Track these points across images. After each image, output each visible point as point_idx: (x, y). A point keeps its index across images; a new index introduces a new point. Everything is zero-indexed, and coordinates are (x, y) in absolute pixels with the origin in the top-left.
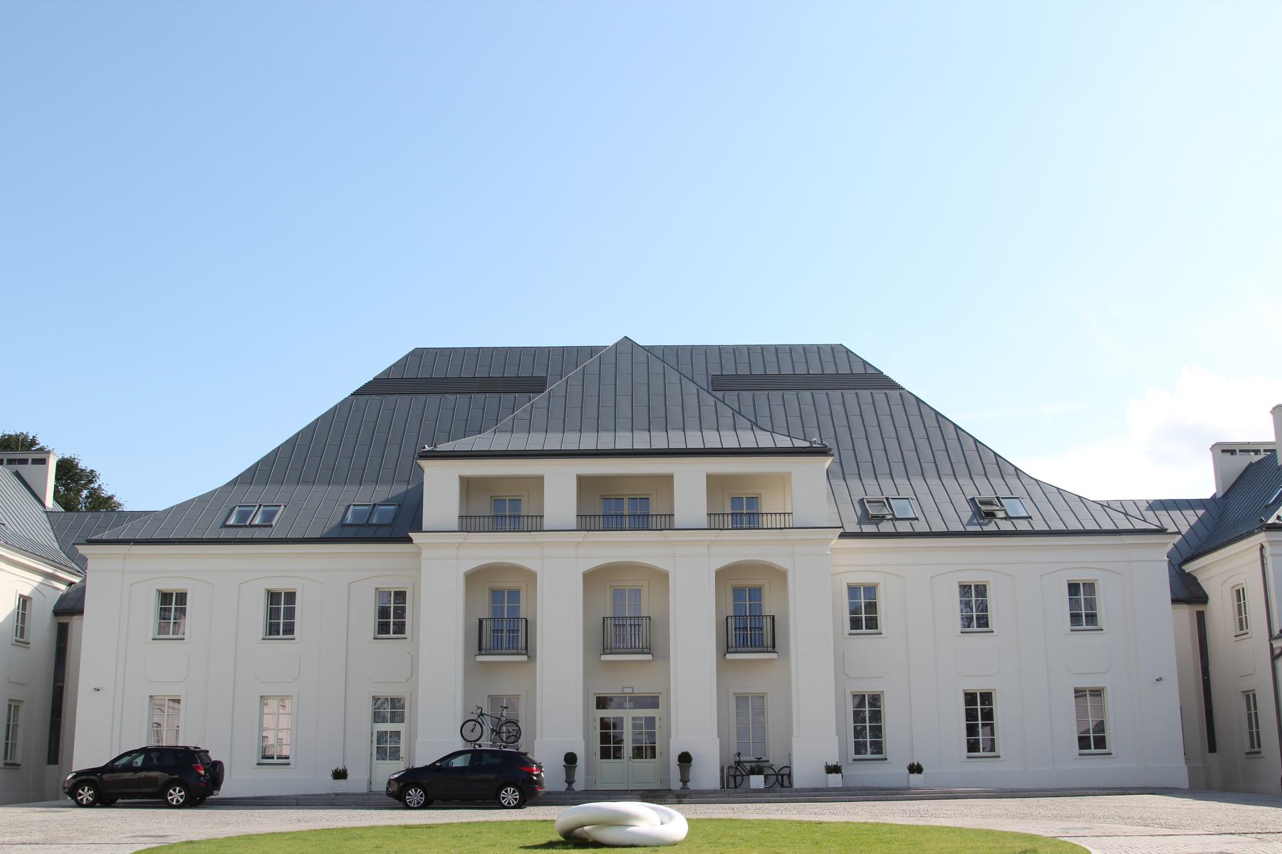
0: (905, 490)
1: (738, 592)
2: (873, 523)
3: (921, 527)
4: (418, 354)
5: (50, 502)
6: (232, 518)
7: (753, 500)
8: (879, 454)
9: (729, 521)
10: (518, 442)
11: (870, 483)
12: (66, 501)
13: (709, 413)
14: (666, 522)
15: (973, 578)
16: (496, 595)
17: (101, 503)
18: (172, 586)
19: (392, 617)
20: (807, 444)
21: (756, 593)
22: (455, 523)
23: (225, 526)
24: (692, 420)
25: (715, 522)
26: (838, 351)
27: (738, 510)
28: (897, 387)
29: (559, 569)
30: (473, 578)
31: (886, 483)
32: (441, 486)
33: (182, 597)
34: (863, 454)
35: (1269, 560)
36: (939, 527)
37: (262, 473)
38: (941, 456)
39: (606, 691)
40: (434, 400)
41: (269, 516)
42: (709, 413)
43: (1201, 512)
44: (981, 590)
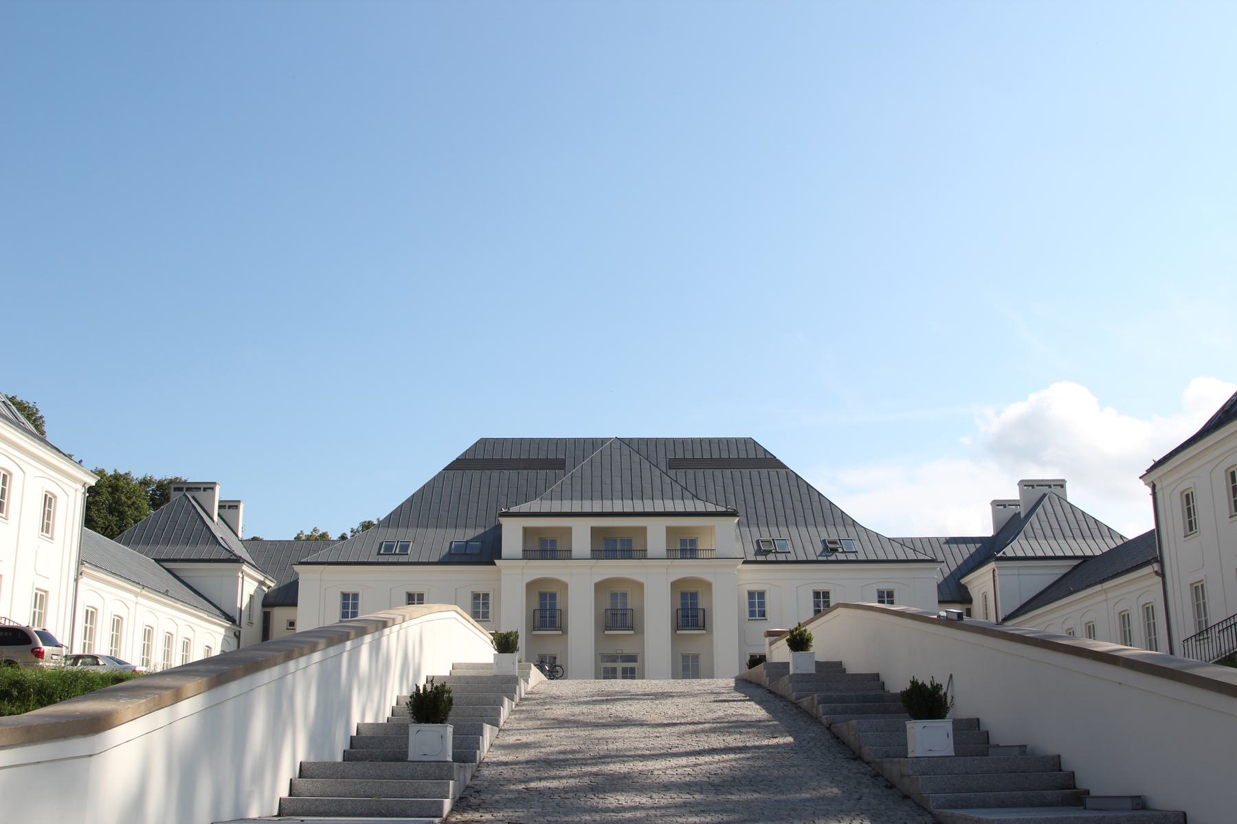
0: (785, 535)
1: (684, 595)
2: (764, 554)
3: (791, 557)
4: (483, 442)
7: (693, 542)
8: (771, 511)
10: (556, 507)
11: (764, 529)
13: (667, 488)
14: (643, 555)
15: (821, 588)
20: (724, 509)
21: (694, 596)
23: (379, 554)
24: (657, 493)
25: (671, 555)
26: (749, 443)
27: (685, 548)
28: (785, 467)
31: (774, 529)
32: (512, 534)
34: (761, 511)
35: (997, 578)
36: (802, 557)
37: (397, 518)
38: (808, 512)
39: (611, 649)
42: (667, 488)
43: (978, 545)
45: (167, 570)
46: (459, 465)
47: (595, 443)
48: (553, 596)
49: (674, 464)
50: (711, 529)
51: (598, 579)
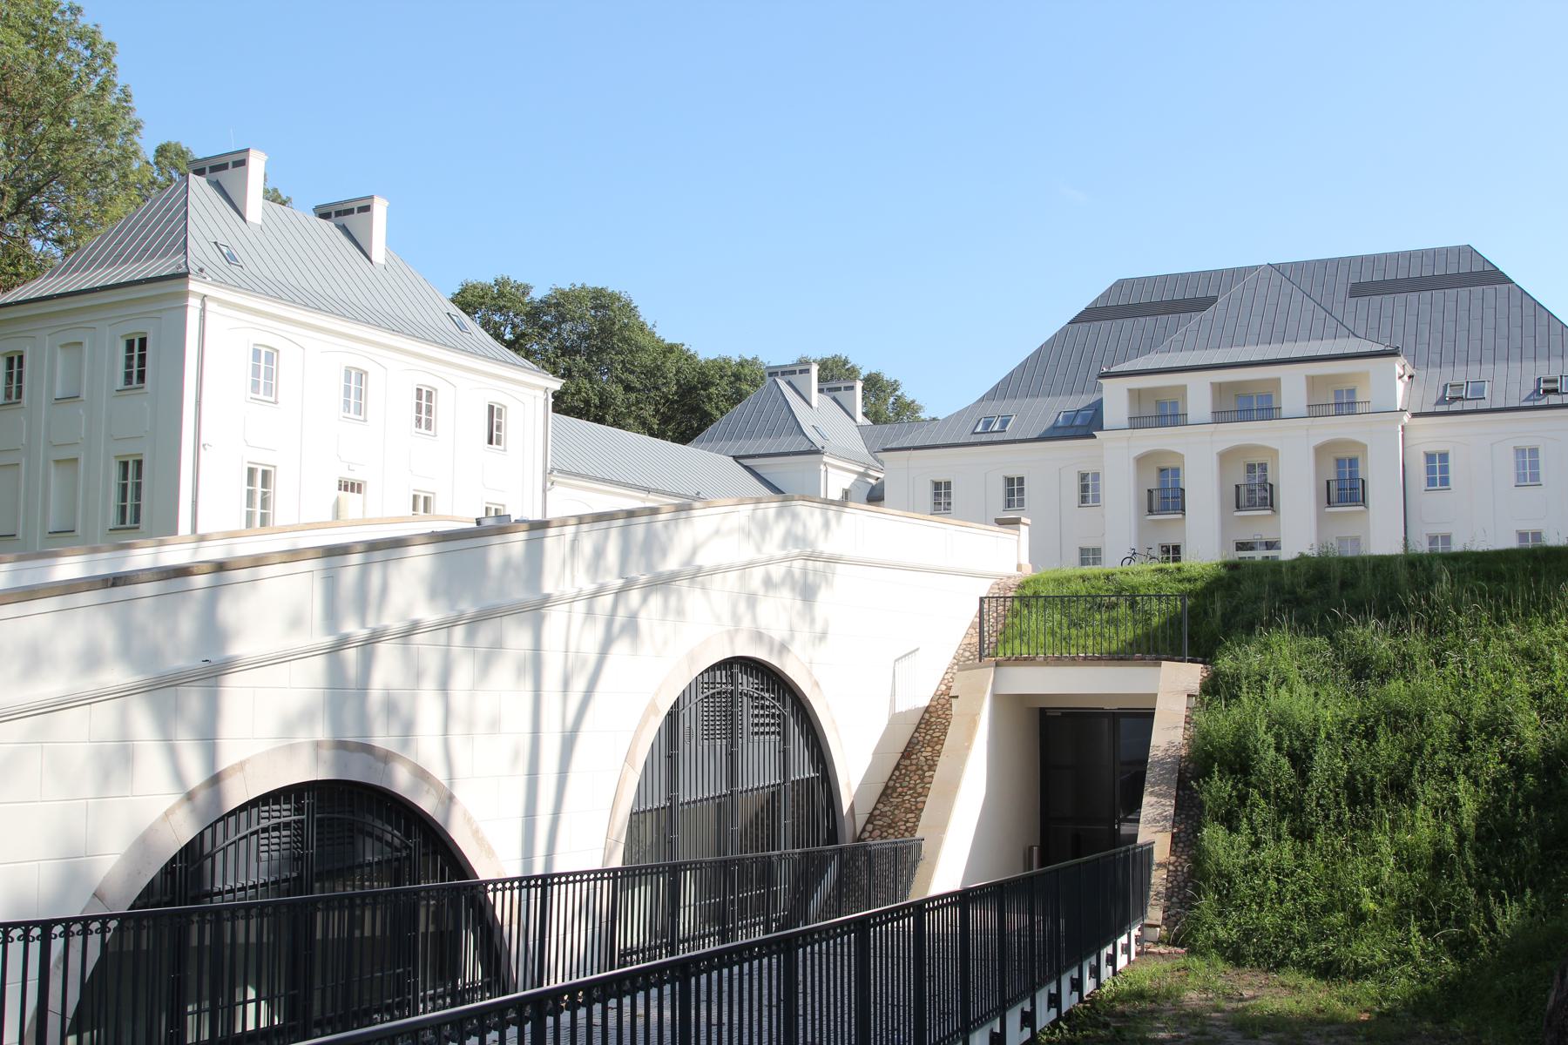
2: (1451, 404)
4: (1120, 284)
5: (860, 418)
6: (983, 428)
7: (1352, 392)
9: (1332, 410)
12: (874, 416)
15: (1526, 443)
16: (1339, 462)
17: (905, 409)
19: (1088, 490)
22: (1126, 424)
26: (1471, 251)
29: (1200, 451)
30: (1321, 451)
32: (1116, 398)
33: (948, 485)
37: (1001, 391)
39: (1245, 537)
40: (1128, 322)
41: (1005, 424)
44: (1534, 452)
45: (746, 467)
46: (1090, 315)
47: (1236, 275)
48: (1263, 467)
49: (1359, 290)
51: (1319, 441)
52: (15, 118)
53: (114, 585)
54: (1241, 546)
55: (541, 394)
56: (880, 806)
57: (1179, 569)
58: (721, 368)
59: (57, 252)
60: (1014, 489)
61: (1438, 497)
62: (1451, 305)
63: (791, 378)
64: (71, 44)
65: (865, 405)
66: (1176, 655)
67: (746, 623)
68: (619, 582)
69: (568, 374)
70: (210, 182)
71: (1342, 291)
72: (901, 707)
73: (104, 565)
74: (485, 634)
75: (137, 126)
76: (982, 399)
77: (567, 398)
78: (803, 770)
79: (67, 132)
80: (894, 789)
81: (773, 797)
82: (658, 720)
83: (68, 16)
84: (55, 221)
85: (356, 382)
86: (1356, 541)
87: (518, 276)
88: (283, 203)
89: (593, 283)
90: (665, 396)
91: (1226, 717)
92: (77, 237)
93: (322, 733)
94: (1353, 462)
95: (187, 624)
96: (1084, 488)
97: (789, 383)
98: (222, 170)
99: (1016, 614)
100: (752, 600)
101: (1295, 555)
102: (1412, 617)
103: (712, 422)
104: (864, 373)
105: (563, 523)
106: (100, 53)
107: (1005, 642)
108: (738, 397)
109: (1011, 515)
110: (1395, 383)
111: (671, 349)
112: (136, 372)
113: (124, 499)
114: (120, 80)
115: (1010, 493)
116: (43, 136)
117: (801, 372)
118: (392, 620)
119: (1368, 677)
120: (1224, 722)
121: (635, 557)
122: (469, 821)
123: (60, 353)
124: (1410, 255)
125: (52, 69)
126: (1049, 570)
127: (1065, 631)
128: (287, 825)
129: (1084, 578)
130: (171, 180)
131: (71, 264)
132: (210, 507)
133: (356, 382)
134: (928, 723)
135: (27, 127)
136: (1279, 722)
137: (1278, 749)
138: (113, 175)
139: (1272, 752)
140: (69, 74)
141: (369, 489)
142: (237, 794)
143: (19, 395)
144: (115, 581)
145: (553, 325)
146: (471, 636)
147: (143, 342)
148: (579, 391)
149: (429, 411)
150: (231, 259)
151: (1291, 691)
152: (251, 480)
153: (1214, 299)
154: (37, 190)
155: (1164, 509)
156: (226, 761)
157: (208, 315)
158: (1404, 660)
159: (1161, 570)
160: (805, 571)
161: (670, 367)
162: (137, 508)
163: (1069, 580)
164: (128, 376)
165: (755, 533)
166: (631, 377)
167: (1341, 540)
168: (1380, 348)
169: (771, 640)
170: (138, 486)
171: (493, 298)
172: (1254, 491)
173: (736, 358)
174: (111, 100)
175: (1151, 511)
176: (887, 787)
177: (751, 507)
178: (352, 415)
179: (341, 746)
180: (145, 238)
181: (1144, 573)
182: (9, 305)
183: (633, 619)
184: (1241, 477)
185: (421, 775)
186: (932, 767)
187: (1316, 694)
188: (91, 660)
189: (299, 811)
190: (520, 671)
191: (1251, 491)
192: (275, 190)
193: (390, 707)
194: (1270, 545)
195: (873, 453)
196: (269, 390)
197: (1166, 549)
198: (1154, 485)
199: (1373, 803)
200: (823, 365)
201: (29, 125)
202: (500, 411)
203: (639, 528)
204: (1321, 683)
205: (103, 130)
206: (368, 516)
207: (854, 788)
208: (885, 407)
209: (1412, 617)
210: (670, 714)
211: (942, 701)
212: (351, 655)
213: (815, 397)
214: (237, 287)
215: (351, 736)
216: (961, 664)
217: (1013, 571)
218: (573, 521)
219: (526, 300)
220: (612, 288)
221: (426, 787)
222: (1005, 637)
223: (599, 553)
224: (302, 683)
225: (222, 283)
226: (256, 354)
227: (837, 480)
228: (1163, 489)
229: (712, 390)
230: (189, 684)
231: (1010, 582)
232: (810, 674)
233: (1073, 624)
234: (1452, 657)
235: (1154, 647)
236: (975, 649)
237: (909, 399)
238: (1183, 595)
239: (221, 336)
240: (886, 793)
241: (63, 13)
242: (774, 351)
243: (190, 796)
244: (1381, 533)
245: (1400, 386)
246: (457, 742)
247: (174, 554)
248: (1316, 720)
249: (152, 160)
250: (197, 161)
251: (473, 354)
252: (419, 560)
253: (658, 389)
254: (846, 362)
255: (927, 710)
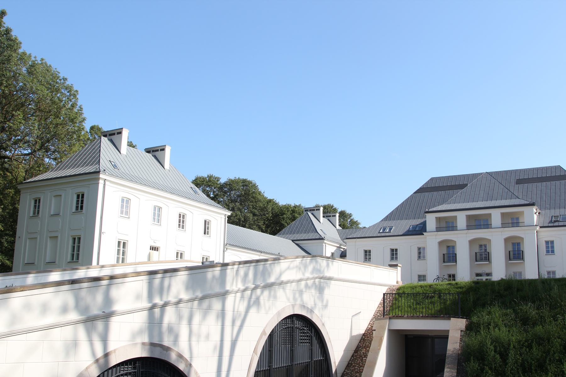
2: (554, 223)
4: (432, 179)
5: (338, 227)
6: (382, 231)
7: (518, 219)
9: (510, 225)
12: (343, 226)
16: (513, 244)
17: (354, 224)
18: (367, 249)
19: (421, 254)
22: (435, 230)
26: (559, 168)
29: (462, 239)
30: (506, 240)
32: (431, 221)
33: (370, 251)
37: (389, 218)
39: (479, 271)
40: (435, 193)
41: (390, 229)
45: (297, 244)
46: (421, 190)
48: (485, 246)
49: (519, 182)
50: (522, 213)
52: (42, 116)
53: (72, 284)
54: (478, 275)
55: (223, 216)
56: (346, 370)
57: (456, 284)
58: (288, 208)
59: (54, 163)
60: (394, 253)
61: (550, 258)
62: (553, 187)
63: (313, 212)
64: (63, 91)
65: (339, 222)
66: (456, 316)
67: (299, 302)
68: (253, 286)
69: (233, 210)
70: (108, 139)
71: (513, 181)
72: (355, 333)
73: (68, 276)
74: (206, 303)
75: (84, 119)
76: (382, 220)
77: (232, 218)
78: (318, 357)
79: (59, 121)
80: (352, 364)
81: (307, 365)
82: (265, 338)
83: (62, 81)
84: (54, 152)
85: (158, 211)
86: (520, 273)
87: (216, 175)
88: (134, 147)
89: (243, 177)
90: (267, 218)
91: (475, 339)
92: (61, 158)
93: (146, 340)
94: (519, 244)
95: (99, 297)
96: (420, 253)
97: (312, 214)
98: (113, 135)
99: (396, 299)
100: (301, 292)
101: (499, 279)
102: (544, 302)
103: (284, 227)
104: (339, 210)
105: (234, 264)
106: (73, 94)
107: (393, 310)
108: (294, 219)
109: (394, 263)
110: (533, 215)
111: (270, 201)
112: (80, 206)
113: (74, 251)
114: (79, 103)
115: (392, 255)
116: (51, 123)
117: (317, 210)
118: (172, 298)
119: (528, 325)
120: (475, 340)
121: (259, 276)
122: (196, 373)
123: (53, 200)
124: (547, 168)
125: (56, 99)
126: (408, 283)
127: (415, 306)
128: (130, 374)
129: (421, 286)
130: (95, 138)
131: (58, 167)
132: (104, 254)
133: (158, 211)
134: (364, 340)
135: (46, 119)
136: (496, 341)
137: (495, 351)
138: (75, 136)
139: (493, 353)
140: (62, 101)
141: (161, 250)
142: (114, 361)
143: (38, 213)
144: (73, 282)
145: (228, 192)
146: (200, 304)
147: (83, 195)
148: (237, 216)
149: (183, 222)
150: (115, 166)
151: (499, 329)
152: (119, 246)
153: (467, 185)
154: (48, 141)
155: (449, 261)
156: (111, 348)
157: (106, 186)
158: (541, 318)
159: (450, 284)
160: (320, 282)
161: (270, 208)
162: (78, 255)
163: (416, 287)
164: (77, 207)
165: (302, 268)
166: (256, 211)
167: (515, 273)
168: (528, 203)
169: (308, 308)
170: (79, 247)
171: (207, 182)
172: (482, 254)
173: (293, 205)
174: (76, 110)
175: (444, 262)
176: (349, 363)
177: (301, 259)
178: (156, 223)
179: (152, 345)
180: (85, 159)
181: (444, 284)
182: (37, 181)
183: (258, 299)
184: (477, 249)
185: (180, 356)
186: (366, 356)
187: (509, 331)
188: (64, 310)
189: (134, 368)
190: (218, 317)
191: (481, 255)
192: (131, 142)
193: (170, 329)
194: (488, 275)
195: (343, 240)
196: (127, 213)
197: (450, 276)
198: (445, 252)
199: (531, 372)
200: (325, 207)
201: (47, 119)
202: (208, 223)
203: (261, 266)
204: (510, 327)
205: (72, 121)
206: (161, 260)
207: (337, 364)
208: (347, 223)
209: (544, 302)
210: (270, 335)
211: (369, 332)
212: (157, 311)
213: (322, 219)
214: (117, 177)
215: (156, 341)
216: (376, 318)
217: (395, 284)
218: (237, 263)
219: (219, 182)
220: (249, 179)
221: (181, 360)
222: (392, 308)
223: (246, 275)
224: (141, 319)
225: (111, 175)
226: (123, 200)
227: (329, 249)
228: (448, 254)
229: (285, 216)
230: (97, 320)
231: (394, 288)
232: (321, 320)
233: (418, 304)
234: (560, 317)
235: (446, 313)
236: (382, 312)
237: (355, 220)
238: (458, 293)
239: (110, 194)
240: (349, 365)
241: (61, 80)
242: (306, 202)
243: (97, 361)
244: (530, 271)
245: (535, 217)
246: (194, 343)
247: (93, 273)
248: (509, 341)
249: (88, 131)
250: (104, 132)
251: (200, 202)
252: (182, 276)
253: (265, 215)
254: (333, 206)
255: (364, 335)
